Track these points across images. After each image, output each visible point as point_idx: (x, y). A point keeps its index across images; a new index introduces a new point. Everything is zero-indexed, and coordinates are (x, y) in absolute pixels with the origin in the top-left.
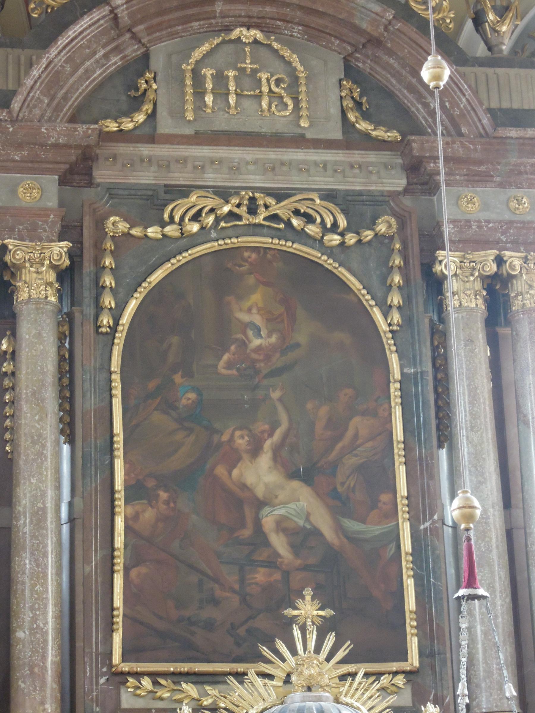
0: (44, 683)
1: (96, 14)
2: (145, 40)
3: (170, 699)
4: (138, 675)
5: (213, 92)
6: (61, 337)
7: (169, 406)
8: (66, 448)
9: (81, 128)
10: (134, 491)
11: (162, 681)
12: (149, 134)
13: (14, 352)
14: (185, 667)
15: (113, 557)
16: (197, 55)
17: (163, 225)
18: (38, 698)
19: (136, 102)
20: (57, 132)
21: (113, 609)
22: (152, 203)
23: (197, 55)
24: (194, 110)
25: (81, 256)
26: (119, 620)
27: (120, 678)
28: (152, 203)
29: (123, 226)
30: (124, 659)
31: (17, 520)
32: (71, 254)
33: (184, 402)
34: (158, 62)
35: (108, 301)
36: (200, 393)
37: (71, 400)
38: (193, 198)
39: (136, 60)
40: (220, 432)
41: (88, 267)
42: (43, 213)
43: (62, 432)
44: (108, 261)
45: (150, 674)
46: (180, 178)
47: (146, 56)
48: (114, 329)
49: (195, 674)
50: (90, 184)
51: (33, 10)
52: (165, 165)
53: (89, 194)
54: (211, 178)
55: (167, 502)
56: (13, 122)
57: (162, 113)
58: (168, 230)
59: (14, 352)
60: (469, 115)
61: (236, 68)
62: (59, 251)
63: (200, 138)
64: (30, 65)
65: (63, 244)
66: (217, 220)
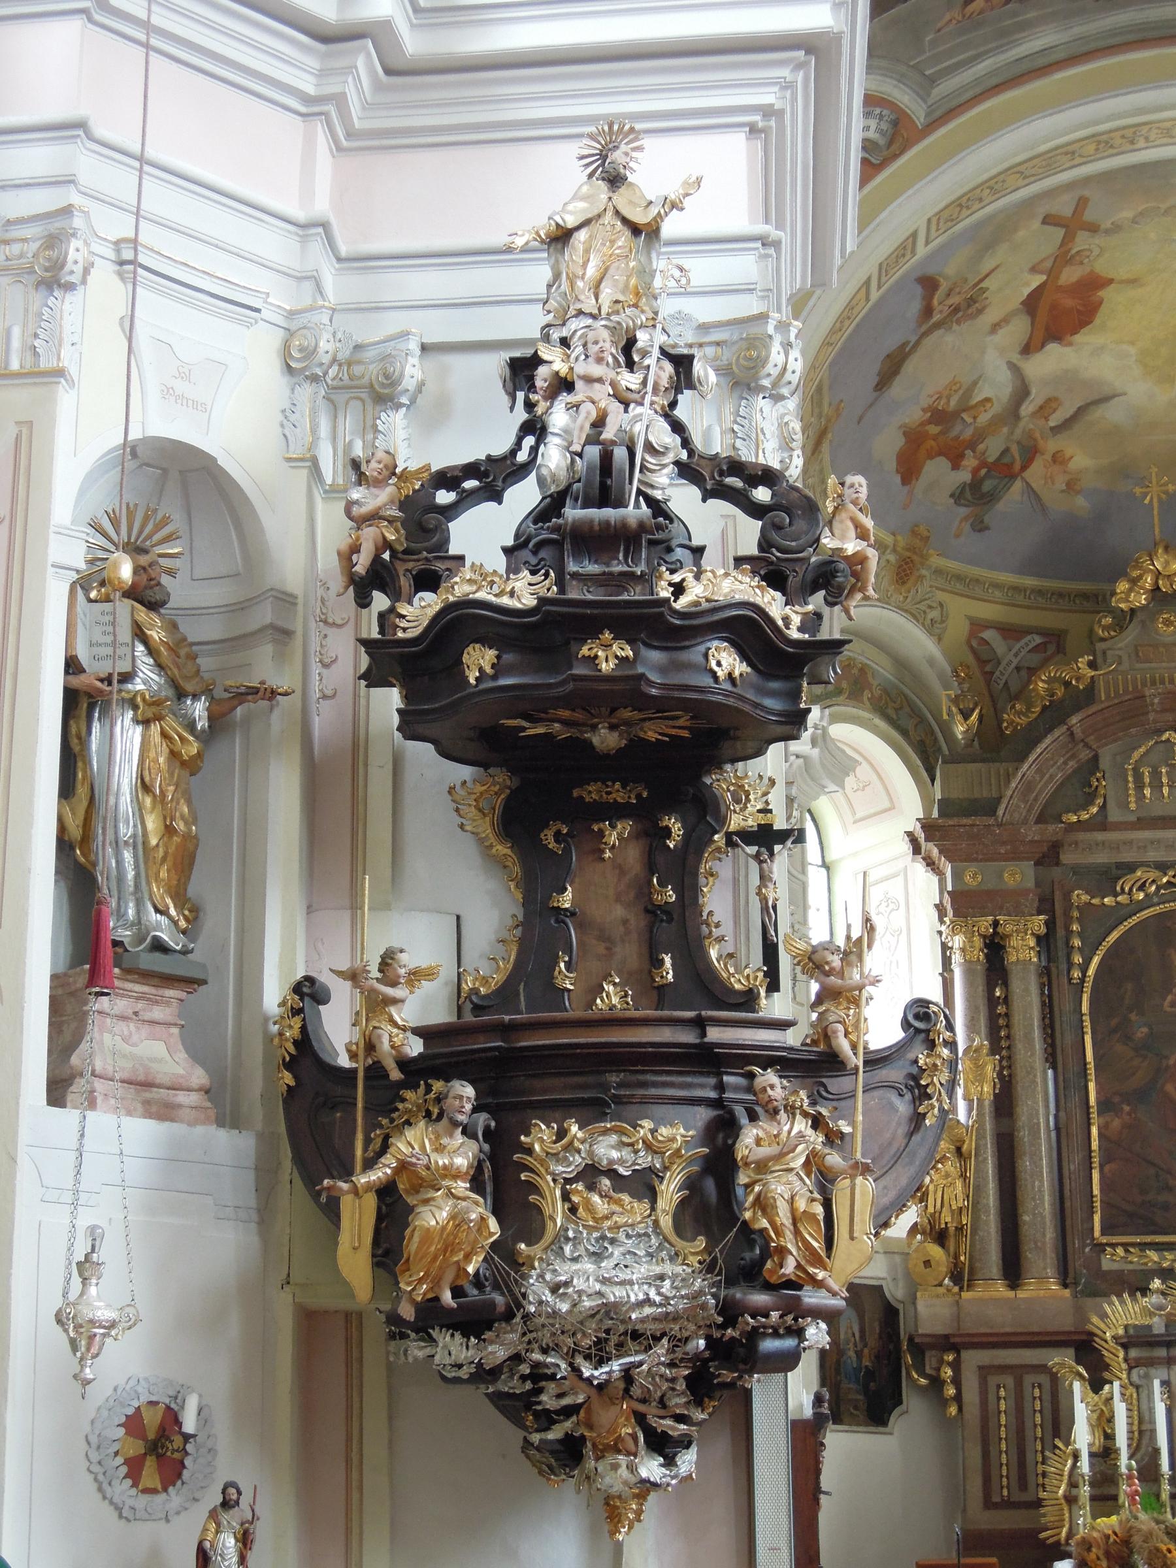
0: (1045, 1253)
1: (1057, 733)
2: (1094, 747)
3: (1138, 1262)
4: (1113, 1246)
5: (1150, 785)
6: (1042, 985)
7: (1127, 1038)
8: (1050, 1072)
9: (1051, 828)
10: (1105, 1106)
11: (1132, 1250)
12: (1101, 823)
13: (1006, 997)
14: (1148, 1239)
15: (1091, 1157)
16: (1136, 755)
17: (1116, 896)
18: (1042, 1265)
19: (1090, 799)
20: (1032, 832)
21: (1092, 1196)
22: (1107, 878)
23: (1136, 755)
24: (1136, 802)
25: (1054, 923)
26: (1098, 1204)
27: (1100, 1248)
28: (1107, 878)
29: (1085, 898)
30: (1103, 1234)
31: (1019, 1131)
32: (1047, 923)
33: (1139, 1035)
34: (1105, 763)
35: (1078, 959)
36: (1151, 1028)
37: (1052, 1036)
38: (1139, 873)
39: (1088, 761)
40: (1167, 1058)
41: (1060, 933)
42: (1026, 892)
43: (1047, 1060)
44: (1075, 927)
45: (1122, 1244)
46: (1127, 857)
47: (1096, 758)
48: (1083, 980)
49: (1157, 1244)
50: (1058, 864)
51: (1006, 728)
52: (1116, 847)
53: (1056, 872)
54: (1153, 855)
55: (1129, 1114)
56: (1000, 825)
57: (1111, 805)
58: (1119, 898)
59: (1006, 997)
60: (1110, 1437)
61: (1167, 765)
62: (1038, 923)
63: (1143, 823)
64: (1008, 778)
65: (1041, 917)
66: (1158, 888)
